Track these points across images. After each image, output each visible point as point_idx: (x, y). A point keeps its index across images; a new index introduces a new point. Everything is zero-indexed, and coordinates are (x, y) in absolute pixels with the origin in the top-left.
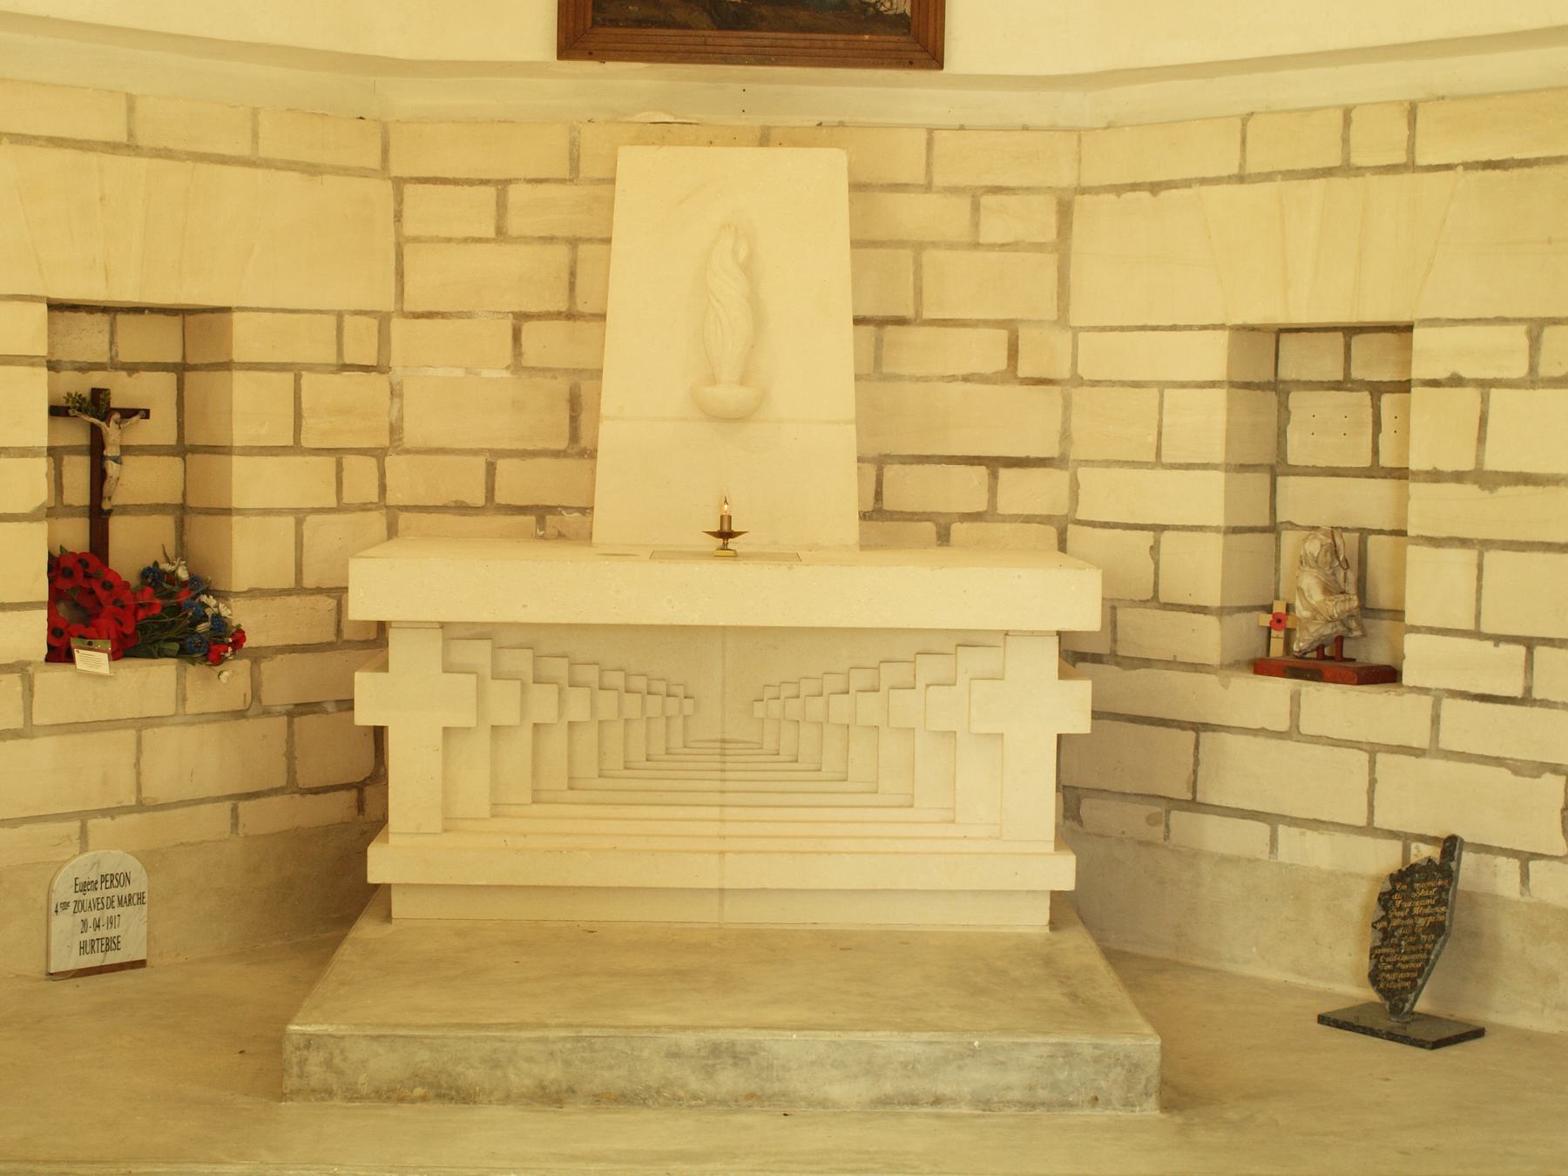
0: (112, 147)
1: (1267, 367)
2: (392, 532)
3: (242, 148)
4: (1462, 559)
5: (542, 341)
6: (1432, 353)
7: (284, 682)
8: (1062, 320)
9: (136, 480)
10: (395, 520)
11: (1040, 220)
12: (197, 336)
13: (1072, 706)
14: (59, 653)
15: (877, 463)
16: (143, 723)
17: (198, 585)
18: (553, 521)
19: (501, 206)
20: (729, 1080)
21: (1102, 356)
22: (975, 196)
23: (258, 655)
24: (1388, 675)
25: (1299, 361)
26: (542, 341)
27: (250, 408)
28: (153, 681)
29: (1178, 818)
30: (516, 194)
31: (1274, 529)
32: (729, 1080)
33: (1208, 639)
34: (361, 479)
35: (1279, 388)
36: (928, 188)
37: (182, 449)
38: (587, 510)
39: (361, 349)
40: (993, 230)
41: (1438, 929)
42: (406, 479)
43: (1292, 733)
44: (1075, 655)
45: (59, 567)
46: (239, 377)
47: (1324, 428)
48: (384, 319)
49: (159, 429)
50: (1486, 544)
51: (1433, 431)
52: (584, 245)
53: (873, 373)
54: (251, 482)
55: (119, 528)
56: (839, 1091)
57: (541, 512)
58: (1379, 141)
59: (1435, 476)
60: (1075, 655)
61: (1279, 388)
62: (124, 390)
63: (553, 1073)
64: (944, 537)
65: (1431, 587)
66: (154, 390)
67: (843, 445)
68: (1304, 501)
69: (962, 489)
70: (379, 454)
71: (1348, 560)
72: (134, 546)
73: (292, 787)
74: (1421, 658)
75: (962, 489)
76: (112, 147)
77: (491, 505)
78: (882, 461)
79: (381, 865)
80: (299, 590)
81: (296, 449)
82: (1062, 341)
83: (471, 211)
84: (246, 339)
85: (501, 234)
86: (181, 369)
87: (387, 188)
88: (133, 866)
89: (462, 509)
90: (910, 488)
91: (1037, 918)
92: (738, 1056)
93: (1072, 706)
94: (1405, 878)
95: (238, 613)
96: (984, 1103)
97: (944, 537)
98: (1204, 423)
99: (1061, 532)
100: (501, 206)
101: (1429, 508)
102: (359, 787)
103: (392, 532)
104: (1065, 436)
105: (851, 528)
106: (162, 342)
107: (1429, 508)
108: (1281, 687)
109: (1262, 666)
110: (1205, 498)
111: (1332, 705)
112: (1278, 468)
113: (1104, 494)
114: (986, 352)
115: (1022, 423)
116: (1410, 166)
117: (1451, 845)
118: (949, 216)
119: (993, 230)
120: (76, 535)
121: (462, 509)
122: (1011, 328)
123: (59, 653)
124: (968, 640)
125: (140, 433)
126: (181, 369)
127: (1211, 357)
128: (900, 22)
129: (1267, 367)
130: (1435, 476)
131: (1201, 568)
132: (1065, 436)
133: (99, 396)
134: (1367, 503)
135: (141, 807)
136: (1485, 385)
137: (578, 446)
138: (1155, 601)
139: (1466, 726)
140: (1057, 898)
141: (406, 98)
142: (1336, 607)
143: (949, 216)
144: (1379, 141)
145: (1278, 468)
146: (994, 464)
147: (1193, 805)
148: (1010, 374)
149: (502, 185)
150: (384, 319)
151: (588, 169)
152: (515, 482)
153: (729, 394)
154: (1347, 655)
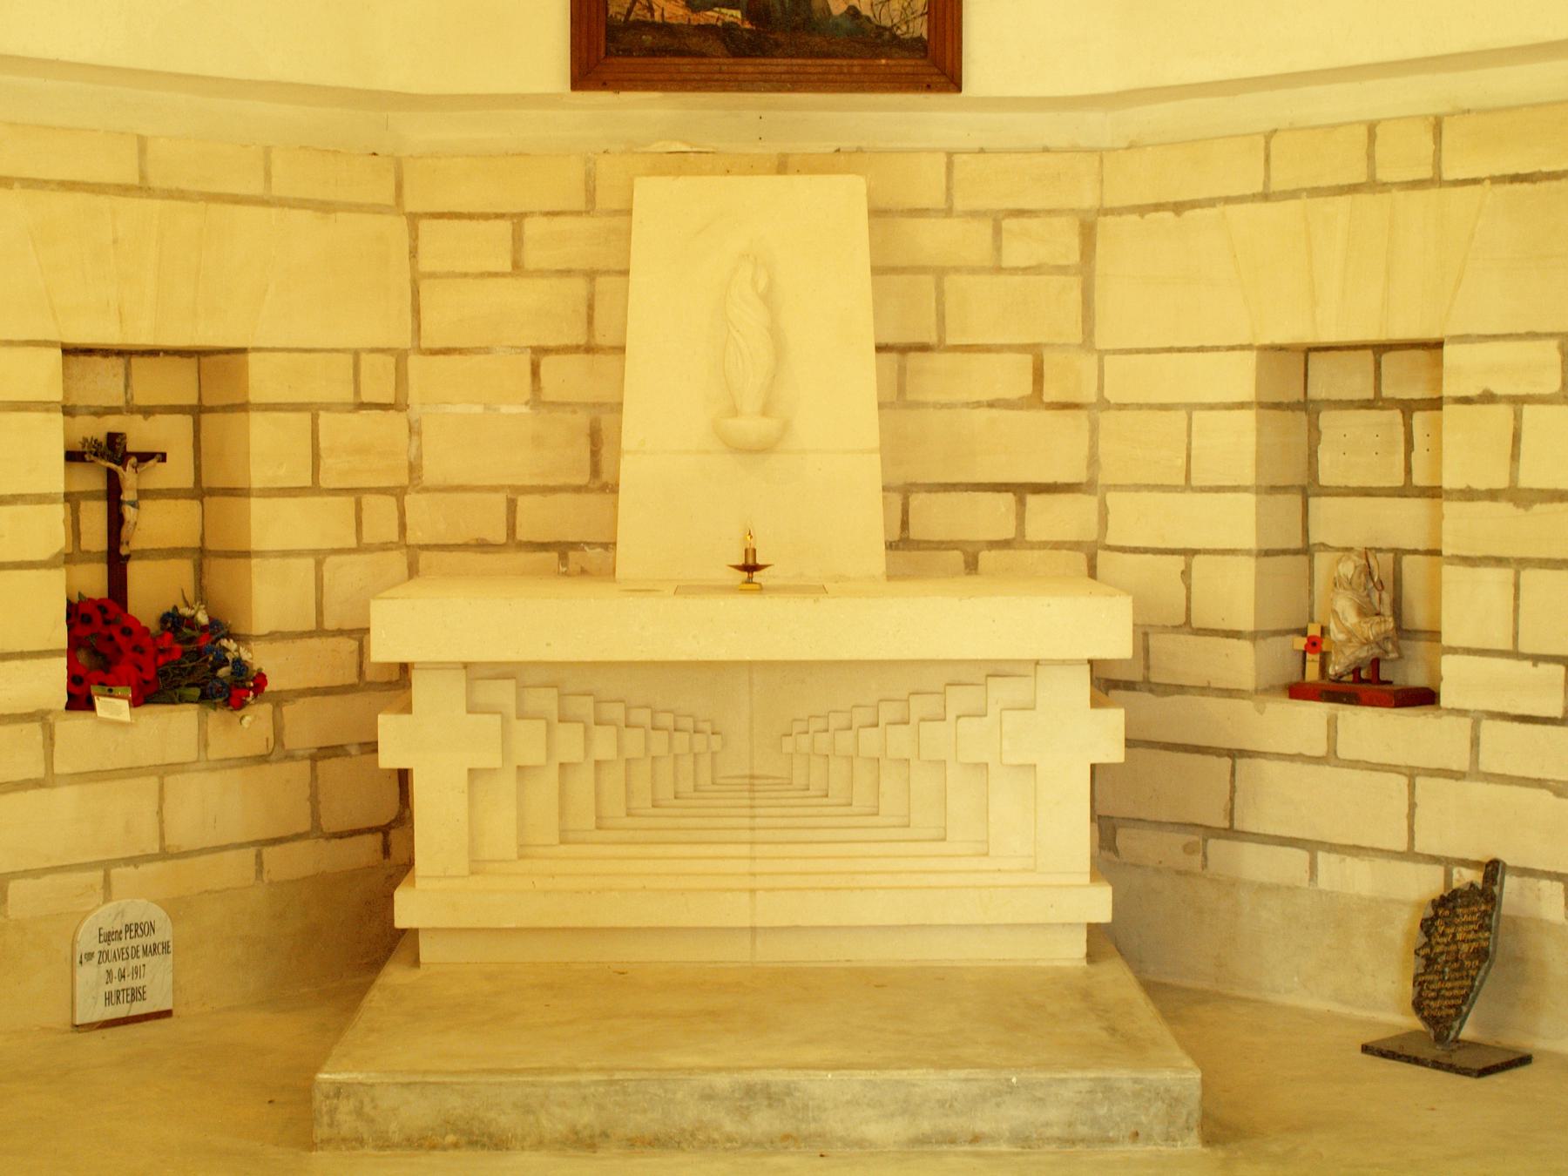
0: (124, 190)
1: (1296, 389)
2: (413, 571)
3: (255, 188)
4: (1495, 580)
5: (562, 376)
6: (1464, 369)
7: (307, 726)
8: (1087, 343)
9: (154, 524)
10: (415, 559)
11: (1063, 244)
12: (213, 377)
13: (1104, 735)
14: (79, 700)
15: (903, 492)
16: (164, 770)
17: (217, 629)
18: (576, 557)
19: (518, 239)
20: (764, 1122)
21: (1124, 379)
22: (997, 219)
23: (280, 699)
24: (1425, 697)
25: (1327, 380)
26: (562, 376)
27: (267, 448)
28: (175, 727)
29: (1216, 847)
30: (532, 227)
31: (1307, 550)
32: (764, 1122)
33: (1242, 664)
34: (381, 519)
35: (1308, 407)
36: (948, 212)
37: (200, 492)
38: (609, 546)
39: (378, 387)
40: (1016, 253)
41: (1482, 955)
42: (426, 518)
43: (1330, 758)
44: (1107, 683)
45: (78, 613)
46: (257, 421)
47: (1354, 447)
48: (400, 357)
49: (175, 471)
50: (1522, 563)
51: (1465, 449)
52: (601, 276)
53: (897, 400)
54: (271, 524)
55: (137, 573)
56: (876, 1130)
57: (563, 549)
58: (1403, 157)
59: (1469, 495)
60: (1107, 683)
61: (1308, 407)
62: (140, 433)
63: (586, 1118)
64: (972, 566)
65: (1467, 607)
66: (169, 434)
67: (869, 474)
68: (1336, 521)
69: (990, 517)
70: (398, 493)
71: (1383, 581)
72: (153, 591)
73: (316, 831)
74: (1458, 679)
75: (990, 517)
76: (124, 190)
77: (513, 543)
78: (907, 490)
79: (408, 909)
80: (319, 632)
81: (315, 489)
82: (1088, 364)
83: (487, 246)
84: (263, 379)
85: (517, 267)
86: (197, 411)
87: (397, 227)
88: (157, 915)
89: (483, 546)
90: (936, 517)
91: (1073, 951)
92: (772, 1097)
93: (1104, 735)
94: (1447, 903)
95: (258, 657)
96: (1023, 1140)
97: (972, 566)
98: (1234, 444)
99: (1091, 558)
100: (518, 239)
101: (1463, 527)
102: (385, 830)
103: (413, 571)
104: (1093, 461)
105: (877, 559)
106: (178, 385)
107: (1463, 527)
108: (1317, 712)
109: (1298, 691)
110: (1236, 521)
111: (1368, 728)
112: (1309, 489)
113: (1133, 519)
114: (1012, 377)
115: (1052, 449)
116: (1436, 181)
117: (1493, 869)
118: (969, 241)
119: (1016, 253)
120: (94, 581)
121: (483, 546)
122: (1036, 353)
123: (79, 700)
124: (998, 670)
125: (157, 477)
126: (197, 411)
127: (1239, 378)
128: (917, 47)
129: (1296, 389)
130: (1469, 495)
131: (1233, 593)
132: (1093, 461)
133: (114, 439)
134: (1400, 522)
135: (164, 855)
136: (1518, 401)
137: (600, 480)
138: (1187, 626)
139: (1507, 748)
140: (1095, 931)
141: (418, 133)
142: (1371, 629)
143: (969, 241)
144: (1403, 157)
145: (1309, 489)
146: (1021, 490)
147: (1231, 833)
148: (1035, 400)
149: (518, 218)
150: (400, 357)
151: (605, 200)
152: (536, 518)
153: (751, 426)
154: (1382, 681)
